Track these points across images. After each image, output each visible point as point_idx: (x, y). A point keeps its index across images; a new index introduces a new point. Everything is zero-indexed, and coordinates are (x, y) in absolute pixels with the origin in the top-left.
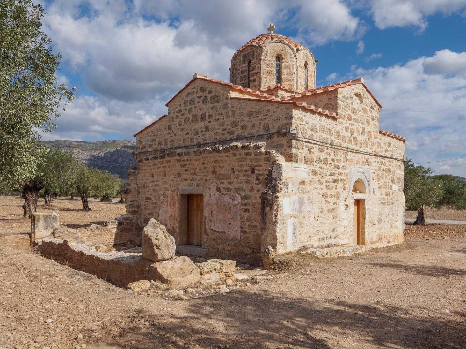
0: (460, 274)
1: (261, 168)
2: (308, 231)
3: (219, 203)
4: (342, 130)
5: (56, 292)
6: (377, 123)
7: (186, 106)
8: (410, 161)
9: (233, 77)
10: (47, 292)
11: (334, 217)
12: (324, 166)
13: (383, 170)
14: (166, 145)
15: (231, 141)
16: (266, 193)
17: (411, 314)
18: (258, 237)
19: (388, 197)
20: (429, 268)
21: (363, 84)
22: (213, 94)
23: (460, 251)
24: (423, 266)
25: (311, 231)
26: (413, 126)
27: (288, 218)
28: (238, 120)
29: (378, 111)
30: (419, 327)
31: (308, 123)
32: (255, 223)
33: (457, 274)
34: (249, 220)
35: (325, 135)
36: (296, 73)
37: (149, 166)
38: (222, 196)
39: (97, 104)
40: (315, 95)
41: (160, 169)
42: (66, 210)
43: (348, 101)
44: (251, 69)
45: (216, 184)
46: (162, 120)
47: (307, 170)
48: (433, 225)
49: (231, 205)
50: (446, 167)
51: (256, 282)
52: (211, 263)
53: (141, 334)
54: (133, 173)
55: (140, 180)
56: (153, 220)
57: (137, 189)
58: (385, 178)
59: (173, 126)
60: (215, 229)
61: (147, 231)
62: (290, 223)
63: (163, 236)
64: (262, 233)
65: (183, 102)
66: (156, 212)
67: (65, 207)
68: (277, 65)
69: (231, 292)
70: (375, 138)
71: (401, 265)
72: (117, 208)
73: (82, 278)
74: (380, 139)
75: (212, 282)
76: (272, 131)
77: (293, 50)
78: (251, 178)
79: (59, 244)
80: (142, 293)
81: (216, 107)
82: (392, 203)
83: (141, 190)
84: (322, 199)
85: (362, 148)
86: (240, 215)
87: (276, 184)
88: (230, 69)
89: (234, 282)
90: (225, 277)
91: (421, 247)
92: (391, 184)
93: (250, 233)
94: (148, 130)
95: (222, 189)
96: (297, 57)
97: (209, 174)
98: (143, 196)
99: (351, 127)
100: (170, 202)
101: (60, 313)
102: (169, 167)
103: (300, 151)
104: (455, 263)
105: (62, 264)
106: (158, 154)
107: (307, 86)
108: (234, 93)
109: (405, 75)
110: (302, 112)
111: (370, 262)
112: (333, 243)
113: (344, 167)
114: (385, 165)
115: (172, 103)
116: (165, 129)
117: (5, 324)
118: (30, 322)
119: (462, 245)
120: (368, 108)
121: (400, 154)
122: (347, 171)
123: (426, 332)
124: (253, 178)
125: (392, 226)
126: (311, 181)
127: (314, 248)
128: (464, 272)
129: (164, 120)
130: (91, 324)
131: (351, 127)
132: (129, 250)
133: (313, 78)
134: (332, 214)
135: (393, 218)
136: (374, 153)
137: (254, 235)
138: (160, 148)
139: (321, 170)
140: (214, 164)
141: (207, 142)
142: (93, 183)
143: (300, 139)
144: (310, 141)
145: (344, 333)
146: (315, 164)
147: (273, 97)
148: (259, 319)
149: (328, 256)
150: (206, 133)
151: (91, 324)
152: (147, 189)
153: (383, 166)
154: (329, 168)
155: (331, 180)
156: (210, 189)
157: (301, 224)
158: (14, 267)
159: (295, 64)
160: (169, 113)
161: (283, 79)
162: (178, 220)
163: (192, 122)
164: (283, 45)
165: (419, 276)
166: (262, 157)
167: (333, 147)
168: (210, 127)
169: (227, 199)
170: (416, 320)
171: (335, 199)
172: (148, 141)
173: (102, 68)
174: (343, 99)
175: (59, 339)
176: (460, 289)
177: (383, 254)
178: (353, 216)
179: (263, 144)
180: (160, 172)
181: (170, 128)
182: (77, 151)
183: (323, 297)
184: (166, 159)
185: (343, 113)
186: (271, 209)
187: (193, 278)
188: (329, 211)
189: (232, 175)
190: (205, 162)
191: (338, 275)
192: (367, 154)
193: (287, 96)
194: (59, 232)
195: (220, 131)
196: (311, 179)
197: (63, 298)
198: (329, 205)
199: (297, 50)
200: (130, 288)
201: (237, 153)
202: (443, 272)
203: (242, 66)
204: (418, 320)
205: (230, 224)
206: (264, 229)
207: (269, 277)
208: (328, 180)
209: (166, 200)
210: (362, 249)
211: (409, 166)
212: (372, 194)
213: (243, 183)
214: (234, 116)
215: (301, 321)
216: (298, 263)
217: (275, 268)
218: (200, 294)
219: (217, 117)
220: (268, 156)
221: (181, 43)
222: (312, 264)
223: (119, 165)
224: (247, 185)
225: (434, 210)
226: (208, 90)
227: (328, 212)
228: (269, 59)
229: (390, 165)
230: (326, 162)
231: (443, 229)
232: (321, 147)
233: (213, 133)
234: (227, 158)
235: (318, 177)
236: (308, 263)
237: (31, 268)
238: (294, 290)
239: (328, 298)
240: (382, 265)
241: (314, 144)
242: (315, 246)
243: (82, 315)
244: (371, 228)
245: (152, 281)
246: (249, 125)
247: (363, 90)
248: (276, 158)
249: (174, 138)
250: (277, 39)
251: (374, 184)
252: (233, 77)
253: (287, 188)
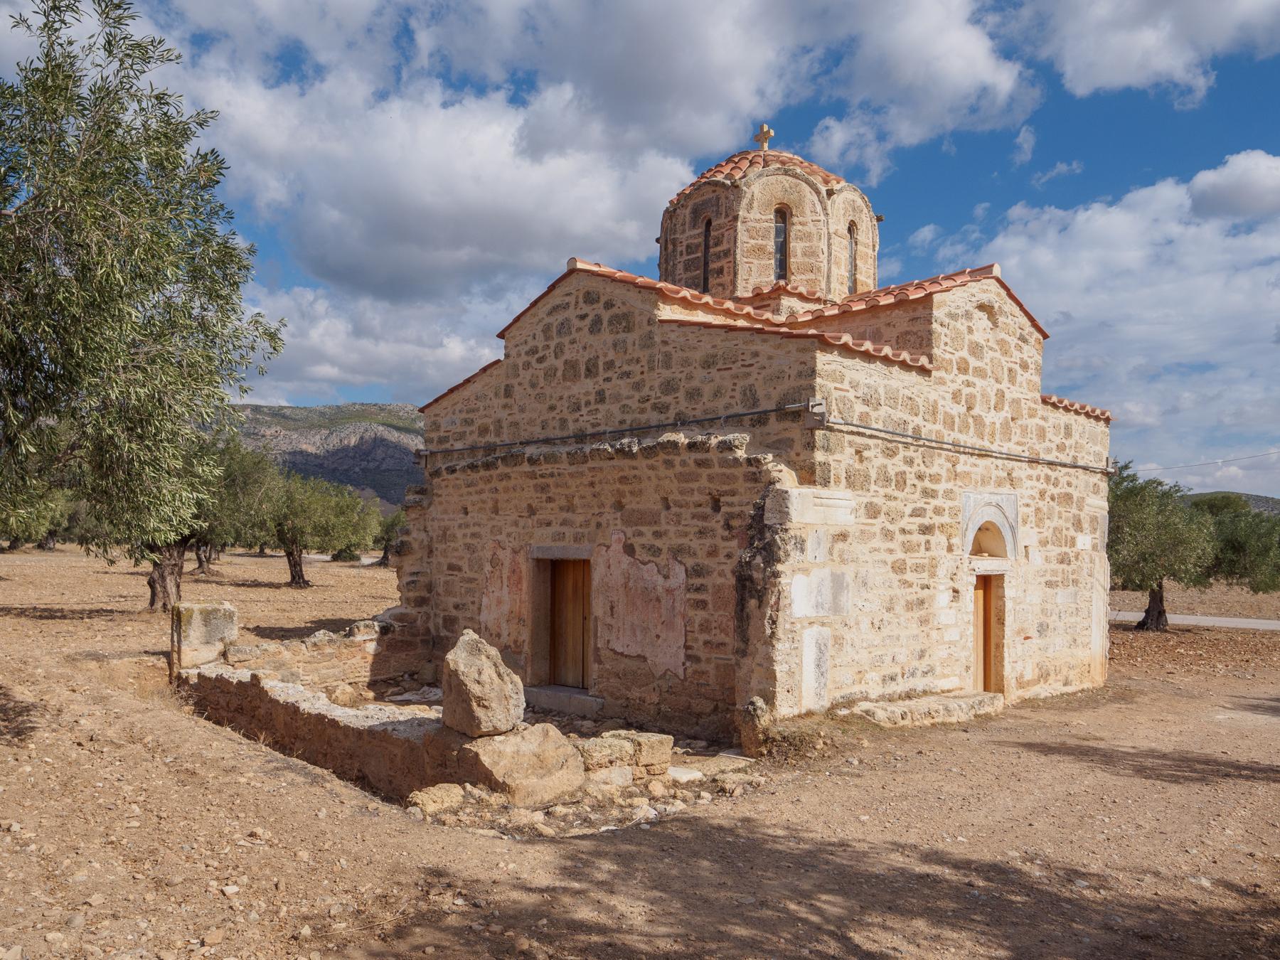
0: (1247, 778)
1: (735, 499)
2: (856, 658)
3: (631, 584)
4: (944, 398)
5: (242, 815)
6: (1036, 379)
7: (548, 338)
8: (1126, 467)
9: (667, 262)
10: (222, 815)
11: (924, 621)
12: (896, 493)
13: (1053, 499)
14: (498, 434)
15: (662, 428)
16: (748, 563)
17: (1111, 889)
18: (728, 671)
19: (1064, 566)
20: (1168, 759)
21: (998, 280)
22: (615, 310)
23: (1255, 708)
24: (1152, 751)
25: (864, 657)
26: (1139, 360)
27: (803, 627)
28: (679, 376)
29: (1037, 346)
30: (1129, 923)
31: (854, 386)
32: (722, 637)
33: (1240, 776)
34: (705, 627)
35: (900, 414)
36: (825, 250)
37: (456, 487)
38: (638, 568)
39: (321, 306)
40: (874, 309)
41: (484, 496)
42: (249, 586)
43: (958, 325)
44: (711, 243)
45: (622, 536)
46: (488, 372)
47: (853, 504)
48: (1189, 631)
49: (660, 589)
50: (1233, 470)
51: (723, 790)
52: (611, 740)
53: (446, 929)
54: (418, 504)
55: (433, 520)
56: (469, 635)
57: (426, 543)
58: (1056, 519)
59: (517, 388)
60: (620, 650)
61: (456, 663)
62: (809, 638)
63: (495, 676)
64: (738, 664)
65: (540, 327)
66: (473, 603)
67: (246, 577)
68: (778, 232)
69: (659, 822)
70: (1031, 416)
71: (1096, 749)
72: (373, 578)
73: (302, 779)
74: (1044, 418)
75: (613, 790)
76: (765, 405)
77: (818, 192)
78: (711, 524)
79: (240, 682)
80: (443, 817)
81: (624, 341)
82: (1075, 582)
83: (436, 545)
84: (892, 575)
85: (996, 444)
87: (775, 540)
88: (658, 240)
89: (667, 788)
90: (647, 777)
91: (1153, 696)
92: (1072, 532)
93: (708, 660)
94: (454, 395)
95: (638, 549)
96: (829, 211)
97: (607, 509)
98: (442, 560)
99: (966, 391)
100: (509, 578)
101: (255, 869)
102: (506, 490)
103: (836, 456)
104: (1240, 742)
105: (248, 738)
106: (480, 458)
107: (855, 282)
108: (668, 307)
109: (1118, 229)
110: (840, 359)
111: (1013, 738)
112: (920, 688)
113: (949, 494)
114: (1056, 485)
115: (514, 331)
116: (496, 395)
117: (131, 897)
118: (189, 892)
119: (1266, 690)
120: (1013, 341)
121: (1097, 455)
122: (956, 503)
123: (1145, 938)
124: (717, 523)
125: (1075, 640)
126: (862, 532)
127: (871, 701)
128: (1260, 770)
129: (494, 371)
130: (329, 901)
131: (966, 391)
132: (406, 696)
133: (871, 261)
134: (917, 614)
135: (1079, 619)
136: (1026, 454)
137: (717, 667)
138: (483, 441)
139: (889, 503)
140: (618, 485)
141: (601, 429)
142: (315, 519)
143: (836, 427)
144: (861, 430)
145: (937, 938)
146: (873, 487)
147: (768, 315)
148: (729, 894)
149: (907, 722)
150: (599, 406)
151: (329, 901)
152: (452, 545)
153: (1051, 487)
154: (910, 496)
155: (915, 527)
156: (608, 547)
157: (838, 641)
158: (139, 746)
159: (825, 229)
160: (507, 356)
161: (793, 267)
162: (529, 622)
163: (564, 378)
164: (795, 180)
165: (1138, 781)
166: (739, 472)
167: (921, 442)
168: (607, 393)
169: (650, 573)
170: (1122, 905)
171: (925, 575)
172: (453, 423)
173: (333, 215)
174: (947, 321)
175: (257, 937)
176: (1242, 820)
177: (1048, 717)
178: (972, 618)
179: (741, 438)
180: (484, 502)
181: (508, 392)
182: (273, 431)
183: (889, 839)
184: (498, 471)
185: (948, 356)
186: (762, 603)
187: (566, 780)
188: (909, 606)
189: (664, 513)
190: (596, 480)
191: (931, 776)
192: (1010, 457)
193: (802, 310)
194: (239, 651)
195: (634, 404)
196: (863, 527)
197: (259, 831)
198: (910, 590)
199: (830, 193)
200: (416, 804)
201: (677, 460)
202: (1203, 771)
203: (688, 233)
204: (1128, 906)
205: (658, 636)
206: (743, 653)
207: (756, 777)
208: (907, 528)
210: (996, 702)
211: (1124, 479)
212: (1023, 560)
213: (691, 536)
214: (667, 365)
215: (832, 904)
216: (829, 742)
217: (770, 752)
218: (585, 820)
219: (626, 368)
220: (753, 469)
221: (535, 145)
222: (866, 743)
223: (378, 467)
224: (703, 541)
225: (1193, 592)
226: (603, 299)
227: (908, 610)
228: (758, 216)
229: (1069, 484)
230: (901, 482)
231: (1215, 644)
232: (889, 445)
233: (615, 408)
234: (651, 473)
235: (881, 521)
236: (855, 742)
237: (181, 751)
238: (816, 817)
239: (902, 841)
240: (1045, 749)
241: (871, 437)
242: (873, 696)
243: (304, 873)
244: (1019, 647)
245: (468, 786)
246: (707, 390)
247: (998, 295)
248: (775, 474)
249: (517, 417)
250: (778, 165)
251: (1028, 535)
252: (667, 262)
253: (802, 550)
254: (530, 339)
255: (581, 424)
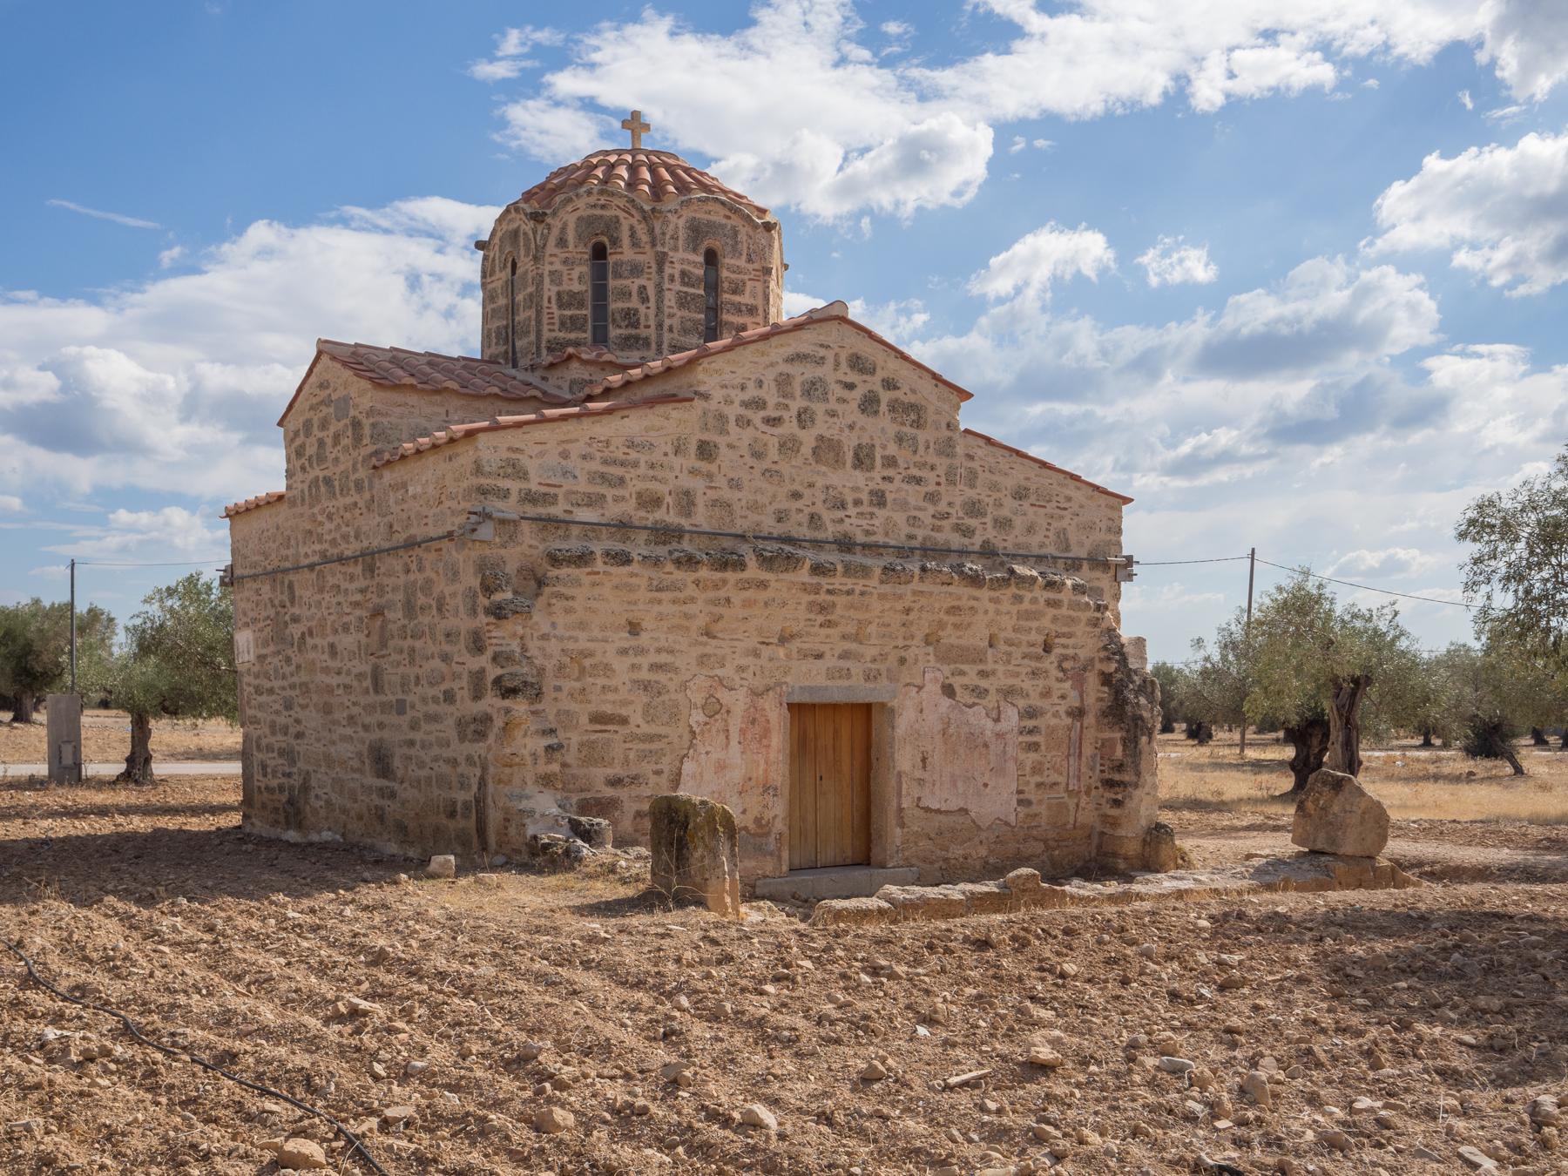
32: (1055, 777)
34: (1037, 769)
38: (962, 712)
49: (988, 733)
60: (935, 806)
86: (1016, 760)
93: (1040, 802)
100: (743, 732)
124: (1050, 663)
137: (1049, 808)
140: (942, 615)
156: (920, 688)
162: (786, 791)
169: (979, 719)
195: (926, 517)
201: (1028, 596)
205: (986, 785)
209: (719, 725)
213: (1023, 677)
219: (915, 472)
233: (900, 518)
234: (991, 607)
254: (751, 385)
255: (846, 526)
